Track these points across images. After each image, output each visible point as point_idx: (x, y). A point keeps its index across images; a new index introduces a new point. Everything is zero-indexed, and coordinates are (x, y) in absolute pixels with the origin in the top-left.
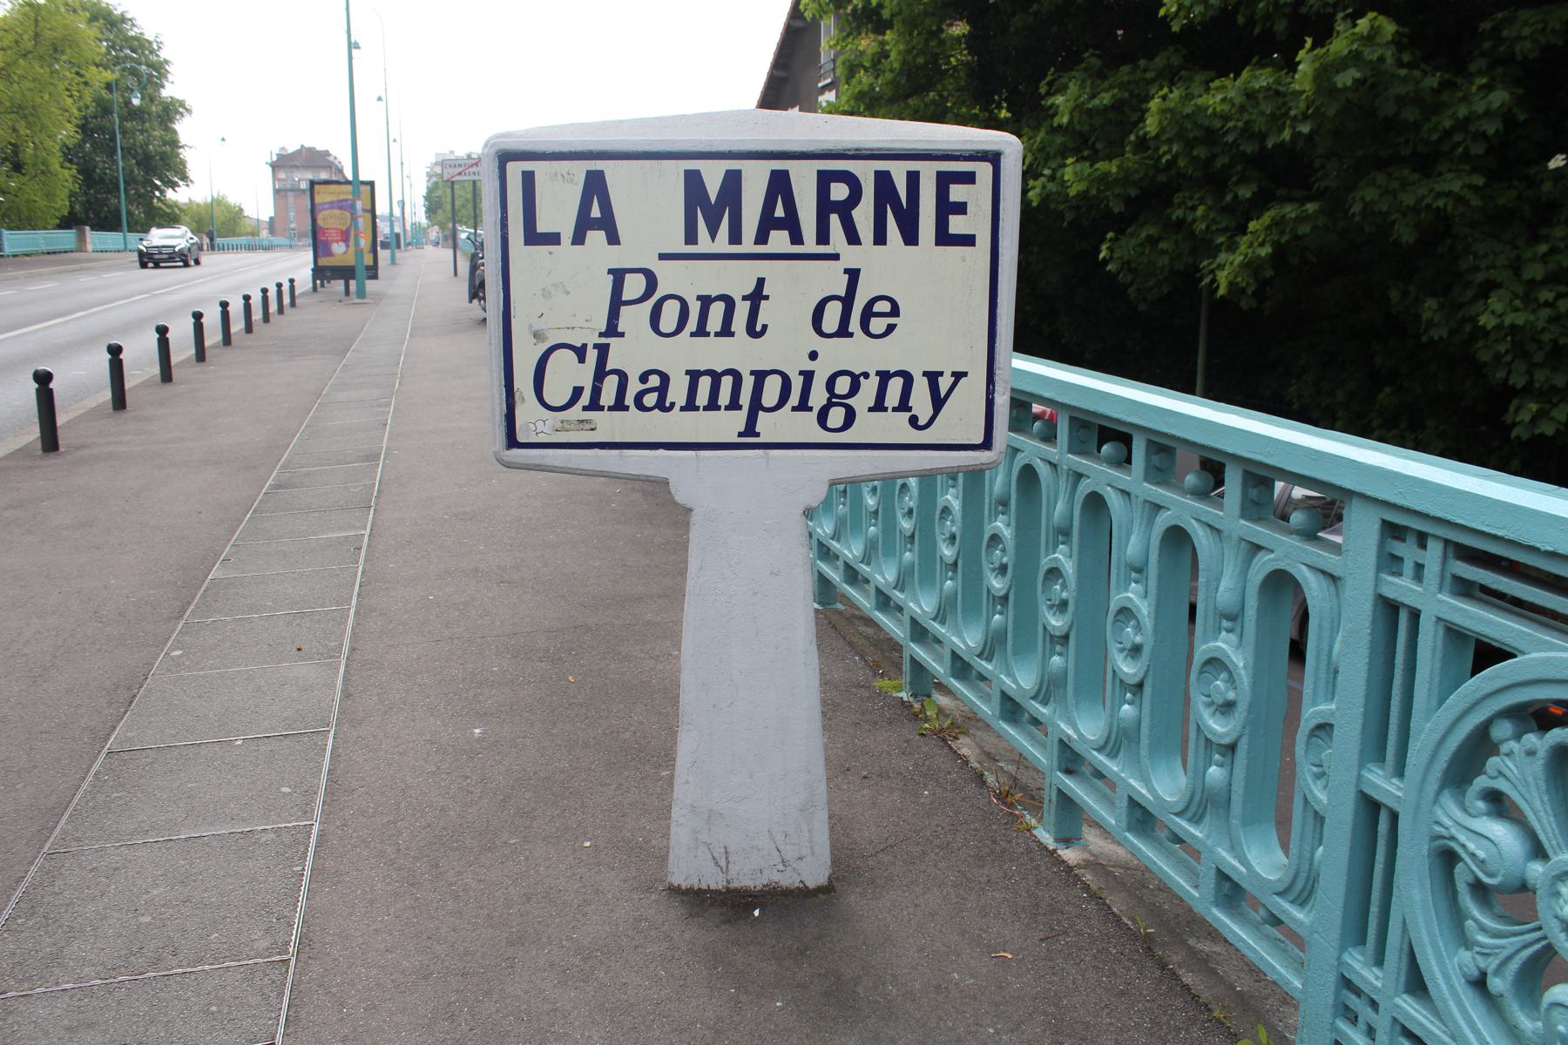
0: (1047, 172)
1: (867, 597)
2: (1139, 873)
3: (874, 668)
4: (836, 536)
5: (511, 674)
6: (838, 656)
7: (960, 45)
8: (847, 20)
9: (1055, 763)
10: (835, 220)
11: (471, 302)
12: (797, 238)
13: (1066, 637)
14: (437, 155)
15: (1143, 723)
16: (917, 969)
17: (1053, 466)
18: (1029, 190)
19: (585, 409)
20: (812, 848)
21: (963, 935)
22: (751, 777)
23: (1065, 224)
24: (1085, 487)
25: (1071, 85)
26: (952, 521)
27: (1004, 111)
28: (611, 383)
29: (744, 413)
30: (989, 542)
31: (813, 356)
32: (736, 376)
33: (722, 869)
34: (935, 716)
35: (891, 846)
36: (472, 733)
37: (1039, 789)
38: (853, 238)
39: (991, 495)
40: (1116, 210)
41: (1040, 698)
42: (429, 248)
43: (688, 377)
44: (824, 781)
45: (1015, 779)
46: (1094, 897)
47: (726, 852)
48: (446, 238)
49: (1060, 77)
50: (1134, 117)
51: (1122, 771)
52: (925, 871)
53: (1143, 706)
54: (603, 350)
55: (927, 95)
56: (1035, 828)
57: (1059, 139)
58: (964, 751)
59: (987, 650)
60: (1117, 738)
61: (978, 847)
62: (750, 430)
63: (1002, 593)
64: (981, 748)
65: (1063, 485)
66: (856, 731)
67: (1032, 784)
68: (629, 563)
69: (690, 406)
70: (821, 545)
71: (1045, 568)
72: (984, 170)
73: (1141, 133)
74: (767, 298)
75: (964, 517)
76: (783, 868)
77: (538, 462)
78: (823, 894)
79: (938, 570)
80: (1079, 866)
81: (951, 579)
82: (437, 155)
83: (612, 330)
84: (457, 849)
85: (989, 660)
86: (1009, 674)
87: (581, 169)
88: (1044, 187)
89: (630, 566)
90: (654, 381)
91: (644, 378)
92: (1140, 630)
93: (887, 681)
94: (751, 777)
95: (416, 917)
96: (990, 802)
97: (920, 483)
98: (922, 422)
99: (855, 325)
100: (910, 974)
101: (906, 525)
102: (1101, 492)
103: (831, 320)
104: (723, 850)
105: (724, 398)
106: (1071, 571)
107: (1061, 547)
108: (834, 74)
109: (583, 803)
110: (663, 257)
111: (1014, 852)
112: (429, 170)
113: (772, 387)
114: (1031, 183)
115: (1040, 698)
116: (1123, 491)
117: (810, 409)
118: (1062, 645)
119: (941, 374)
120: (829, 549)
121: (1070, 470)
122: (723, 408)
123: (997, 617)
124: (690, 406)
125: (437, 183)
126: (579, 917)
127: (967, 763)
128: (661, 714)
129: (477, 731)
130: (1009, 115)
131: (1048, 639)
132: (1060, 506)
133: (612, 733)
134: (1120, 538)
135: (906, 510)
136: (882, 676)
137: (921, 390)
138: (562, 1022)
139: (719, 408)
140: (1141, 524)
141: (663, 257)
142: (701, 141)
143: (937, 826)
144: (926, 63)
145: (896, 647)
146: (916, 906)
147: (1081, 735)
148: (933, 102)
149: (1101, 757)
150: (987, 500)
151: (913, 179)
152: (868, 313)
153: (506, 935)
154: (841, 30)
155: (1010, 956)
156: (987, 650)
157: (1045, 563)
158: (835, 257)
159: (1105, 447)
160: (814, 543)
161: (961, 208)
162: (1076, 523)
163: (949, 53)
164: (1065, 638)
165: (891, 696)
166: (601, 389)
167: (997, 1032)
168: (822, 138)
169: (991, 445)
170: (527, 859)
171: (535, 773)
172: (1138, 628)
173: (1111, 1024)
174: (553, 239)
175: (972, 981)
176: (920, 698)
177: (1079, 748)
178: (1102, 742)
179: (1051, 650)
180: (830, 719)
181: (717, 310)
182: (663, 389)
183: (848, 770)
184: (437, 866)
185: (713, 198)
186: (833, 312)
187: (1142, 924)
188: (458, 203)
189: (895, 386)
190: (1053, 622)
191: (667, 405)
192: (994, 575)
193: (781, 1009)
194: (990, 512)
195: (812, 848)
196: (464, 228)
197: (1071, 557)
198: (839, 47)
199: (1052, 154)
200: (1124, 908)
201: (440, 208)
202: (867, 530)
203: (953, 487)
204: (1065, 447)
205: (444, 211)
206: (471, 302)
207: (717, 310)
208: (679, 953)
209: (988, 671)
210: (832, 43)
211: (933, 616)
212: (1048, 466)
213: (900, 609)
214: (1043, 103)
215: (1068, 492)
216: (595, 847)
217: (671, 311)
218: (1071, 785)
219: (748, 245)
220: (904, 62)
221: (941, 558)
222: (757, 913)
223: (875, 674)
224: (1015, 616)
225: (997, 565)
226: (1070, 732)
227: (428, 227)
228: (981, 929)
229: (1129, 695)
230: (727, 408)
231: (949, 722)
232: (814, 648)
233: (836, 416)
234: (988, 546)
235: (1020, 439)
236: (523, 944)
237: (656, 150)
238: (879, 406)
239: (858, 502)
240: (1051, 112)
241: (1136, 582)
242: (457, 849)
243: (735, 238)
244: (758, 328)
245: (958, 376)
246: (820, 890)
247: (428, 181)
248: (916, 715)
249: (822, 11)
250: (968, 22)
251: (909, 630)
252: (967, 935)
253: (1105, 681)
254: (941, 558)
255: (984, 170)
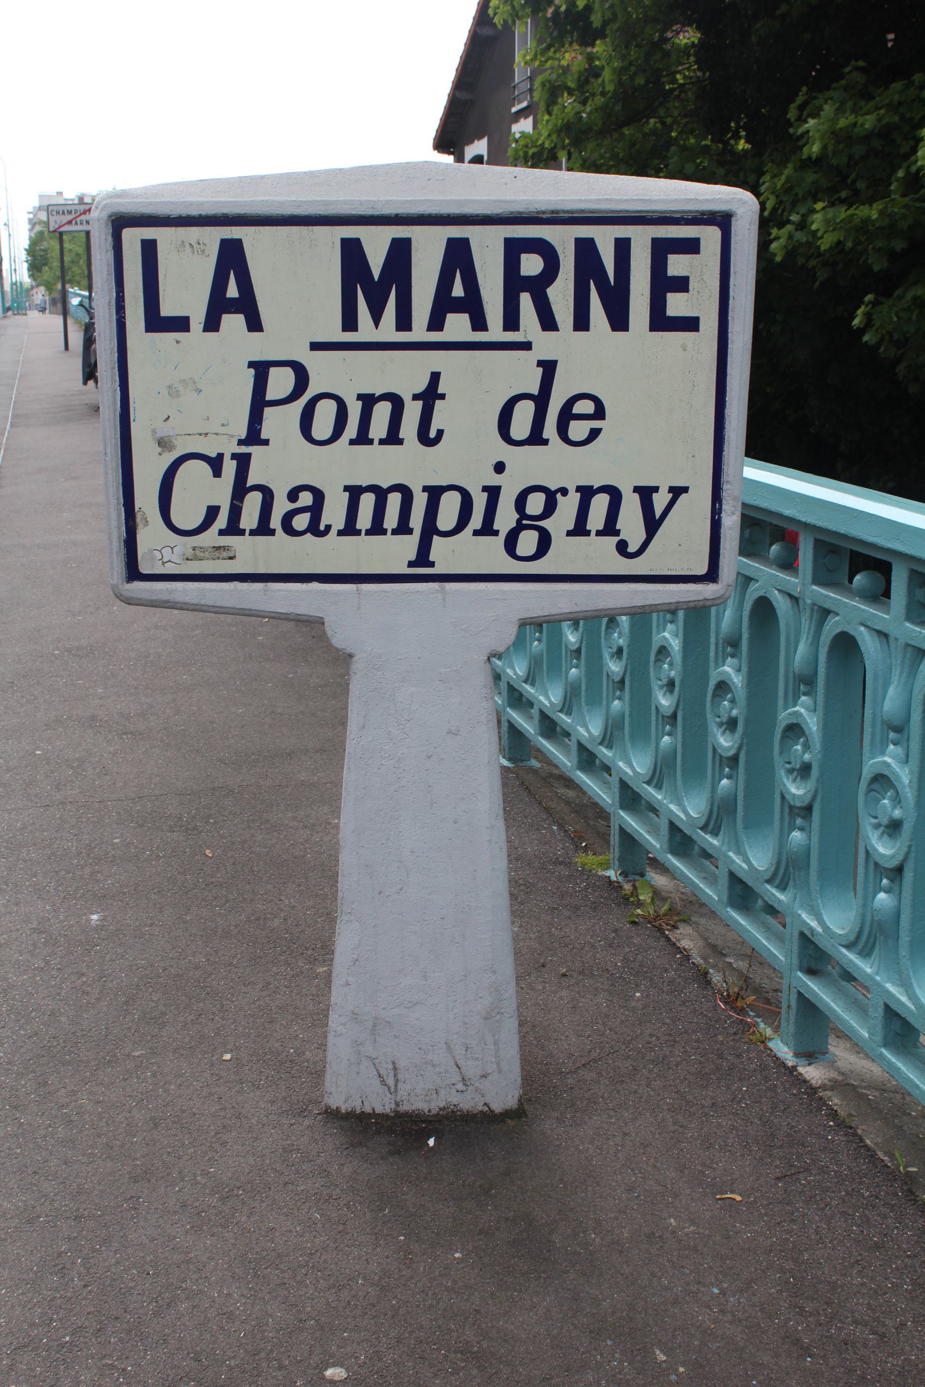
0: (794, 218)
1: (567, 752)
2: (899, 1096)
3: (576, 839)
4: (530, 678)
5: (136, 847)
6: (531, 825)
7: (688, 59)
8: (547, 27)
9: (795, 961)
10: (526, 300)
11: (85, 383)
12: (479, 323)
13: (809, 809)
14: (41, 197)
15: (902, 916)
16: (625, 1213)
17: (794, 599)
18: (772, 241)
19: (222, 533)
20: (498, 1064)
21: (682, 1171)
22: (425, 977)
23: (817, 284)
24: (832, 626)
25: (827, 107)
26: (671, 664)
27: (742, 141)
28: (253, 502)
29: (416, 537)
30: (715, 690)
31: (500, 468)
32: (406, 492)
33: (389, 1088)
34: (649, 901)
35: (595, 1061)
36: (89, 920)
37: (776, 991)
38: (548, 322)
39: (717, 632)
40: (876, 268)
41: (777, 882)
42: (34, 315)
43: (347, 494)
44: (513, 983)
45: (746, 979)
46: (842, 1125)
47: (395, 1069)
48: (54, 302)
49: (815, 98)
50: (905, 148)
51: (877, 974)
52: (635, 1092)
53: (903, 895)
54: (243, 461)
55: (647, 122)
56: (770, 1039)
57: (810, 177)
58: (685, 943)
59: (712, 822)
60: (870, 932)
61: (701, 1063)
62: (423, 557)
63: (732, 753)
64: (706, 939)
65: (806, 624)
66: (553, 918)
67: (767, 984)
68: (279, 710)
69: (350, 529)
70: (511, 689)
71: (784, 724)
72: (710, 236)
73: (913, 169)
74: (442, 397)
75: (685, 659)
76: (464, 1088)
77: (164, 597)
78: (512, 1119)
79: (653, 723)
80: (824, 1087)
81: (669, 734)
82: (41, 197)
83: (254, 437)
84: (69, 1063)
85: (715, 833)
86: (740, 851)
87: (214, 236)
88: (790, 237)
89: (281, 714)
90: (306, 499)
91: (293, 495)
92: (900, 802)
93: (591, 857)
94: (425, 977)
95: (19, 1146)
96: (716, 1006)
97: (631, 620)
98: (632, 549)
99: (550, 430)
100: (617, 1218)
101: (615, 667)
102: (852, 633)
103: (521, 426)
104: (391, 1066)
105: (391, 520)
106: (815, 728)
107: (803, 698)
108: (532, 97)
109: (222, 1006)
110: (316, 347)
111: (745, 1069)
112: (31, 216)
113: (450, 506)
114: (774, 232)
115: (777, 882)
116: (879, 632)
117: (496, 533)
118: (804, 818)
119: (656, 489)
120: (521, 695)
121: (814, 604)
122: (389, 532)
123: (725, 781)
124: (350, 529)
125: (41, 233)
126: (217, 1146)
127: (688, 957)
128: (316, 896)
129: (95, 917)
130: (748, 146)
131: (787, 810)
132: (802, 649)
133: (258, 919)
134: (875, 689)
135: (615, 650)
136: (585, 849)
137: (631, 509)
138: (195, 1276)
139: (384, 532)
140: (901, 673)
141: (316, 347)
142: (361, 203)
143: (651, 1035)
144: (647, 82)
145: (602, 814)
146: (625, 1134)
147: (826, 928)
148: (654, 132)
149: (851, 956)
150: (713, 640)
151: (623, 247)
152: (566, 416)
153: (127, 1169)
154: (540, 41)
155: (739, 1198)
156: (712, 822)
157: (783, 717)
158: (526, 346)
159: (858, 578)
160: (503, 685)
161: (682, 285)
162: (822, 670)
163: (673, 69)
164: (808, 810)
165: (596, 875)
166: (241, 508)
167: (723, 1292)
168: (508, 198)
169: (717, 576)
170: (154, 1075)
171: (165, 969)
172: (897, 800)
173: (863, 1284)
174: (181, 324)
175: (692, 1228)
176: (631, 877)
177: (825, 944)
178: (852, 938)
179: (790, 823)
180: (521, 903)
181: (382, 411)
182: (316, 509)
183: (543, 966)
184: (45, 1083)
185: (376, 273)
186: (524, 414)
187: (902, 1161)
188: (67, 259)
189: (600, 505)
190: (793, 790)
191: (322, 528)
192: (721, 730)
193: (460, 1260)
194: (717, 653)
195: (498, 1064)
196: (76, 290)
197: (815, 711)
198: (537, 63)
199: (800, 196)
200: (879, 1140)
201: (45, 264)
202: (567, 673)
203: (671, 622)
204: (809, 577)
205: (51, 268)
206: (85, 383)
207: (382, 411)
208: (338, 1191)
209: (714, 847)
210: (528, 58)
211: (647, 779)
212: (788, 600)
213: (607, 769)
214: (791, 130)
215: (812, 631)
216: (236, 1060)
217: (325, 414)
218: (814, 987)
219: (419, 332)
220: (620, 83)
221: (657, 709)
222: (431, 1142)
223: (577, 848)
224: (747, 781)
225: (724, 720)
226: (814, 924)
227: (32, 288)
228: (703, 1165)
229: (885, 881)
230: (394, 532)
231: (666, 907)
232: (501, 824)
233: (528, 542)
234: (715, 695)
235: (753, 566)
236: (149, 1181)
237: (306, 213)
238: (580, 529)
239: (556, 639)
240: (800, 143)
241: (894, 744)
242: (69, 1063)
243: (404, 322)
244: (433, 434)
245: (677, 492)
246: (508, 1114)
247: (31, 230)
248: (626, 898)
249: (515, 15)
250: (698, 28)
251: (618, 794)
252: (686, 1172)
253: (856, 866)
254: (657, 709)
255: (710, 236)
